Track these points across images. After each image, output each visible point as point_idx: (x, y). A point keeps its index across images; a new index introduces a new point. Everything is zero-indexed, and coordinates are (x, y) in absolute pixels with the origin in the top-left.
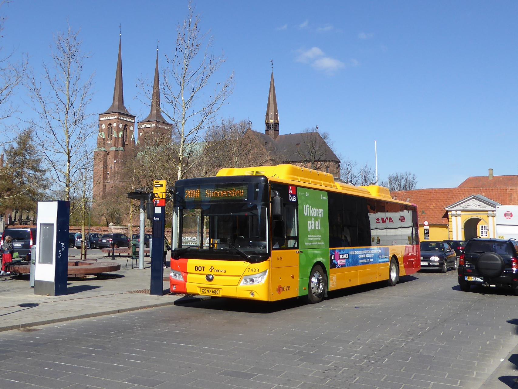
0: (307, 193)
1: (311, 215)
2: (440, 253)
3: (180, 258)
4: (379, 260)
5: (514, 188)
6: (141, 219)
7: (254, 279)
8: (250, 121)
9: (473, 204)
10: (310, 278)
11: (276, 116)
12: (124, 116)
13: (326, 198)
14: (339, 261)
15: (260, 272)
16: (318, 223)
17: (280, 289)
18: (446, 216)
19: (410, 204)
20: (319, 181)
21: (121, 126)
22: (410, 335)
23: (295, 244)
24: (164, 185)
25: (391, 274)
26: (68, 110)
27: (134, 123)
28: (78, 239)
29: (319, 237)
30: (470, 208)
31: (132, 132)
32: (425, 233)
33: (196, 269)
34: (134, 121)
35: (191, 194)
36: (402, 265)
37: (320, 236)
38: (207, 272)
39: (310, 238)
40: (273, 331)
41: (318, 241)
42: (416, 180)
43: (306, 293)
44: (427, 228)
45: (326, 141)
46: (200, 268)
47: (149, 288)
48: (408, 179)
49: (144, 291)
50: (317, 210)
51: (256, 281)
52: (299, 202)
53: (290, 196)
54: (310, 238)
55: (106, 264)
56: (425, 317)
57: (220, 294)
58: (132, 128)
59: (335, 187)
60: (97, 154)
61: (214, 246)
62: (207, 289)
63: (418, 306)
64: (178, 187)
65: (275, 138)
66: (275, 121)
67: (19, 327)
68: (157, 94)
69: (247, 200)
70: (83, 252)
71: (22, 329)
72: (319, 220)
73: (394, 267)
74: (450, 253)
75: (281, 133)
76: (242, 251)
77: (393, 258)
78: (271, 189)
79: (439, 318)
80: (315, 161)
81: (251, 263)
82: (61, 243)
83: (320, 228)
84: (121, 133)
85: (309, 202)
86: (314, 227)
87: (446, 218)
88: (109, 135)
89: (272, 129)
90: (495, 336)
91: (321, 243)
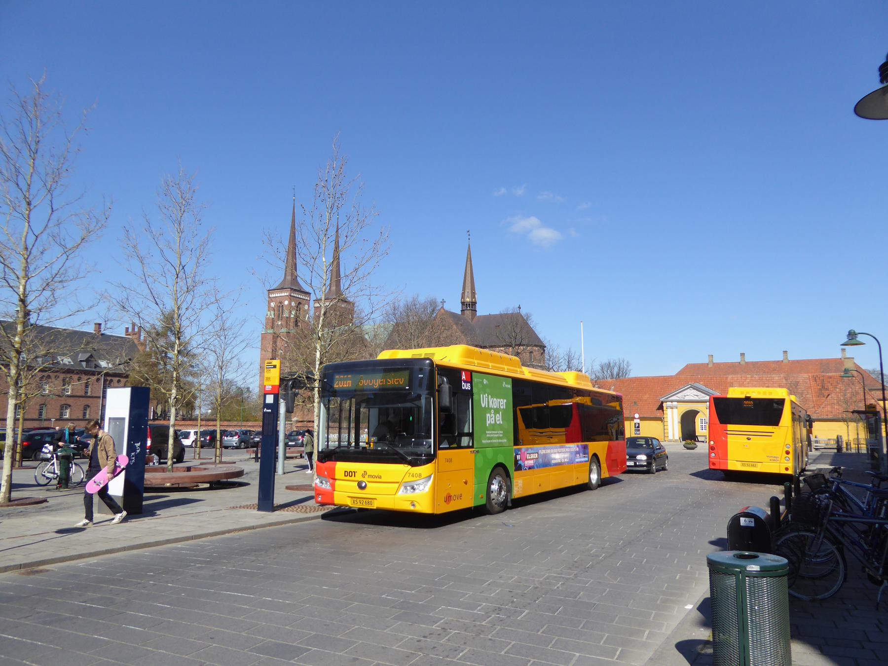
0: (485, 380)
1: (490, 407)
2: (648, 451)
3: (327, 461)
4: (577, 460)
5: (734, 376)
6: (280, 412)
7: (415, 486)
8: (443, 300)
9: (690, 394)
10: (490, 483)
11: (473, 294)
12: (297, 293)
13: (509, 386)
14: (526, 462)
15: (422, 478)
16: (499, 417)
17: (448, 499)
18: (661, 407)
19: (614, 393)
20: (502, 366)
21: (293, 304)
22: (576, 567)
23: (469, 443)
24: (278, 367)
25: (591, 476)
26: (179, 273)
27: (309, 301)
28: (225, 437)
29: (501, 434)
30: (687, 398)
31: (307, 312)
32: (635, 427)
33: (346, 475)
34: (309, 299)
35: (342, 383)
36: (604, 465)
37: (502, 432)
38: (359, 477)
39: (489, 434)
40: (386, 566)
41: (499, 438)
42: (630, 368)
43: (483, 502)
44: (638, 421)
45: (529, 322)
46: (351, 473)
47: (256, 501)
48: (622, 366)
49: (247, 507)
50: (499, 400)
51: (418, 489)
52: (475, 390)
53: (463, 383)
54: (489, 434)
55: (225, 469)
56: (605, 538)
57: (375, 505)
58: (306, 307)
59: (522, 373)
60: (264, 337)
61: (370, 445)
62: (358, 500)
63: (602, 521)
64: (327, 372)
65: (472, 319)
66: (472, 300)
67: (20, 566)
68: (293, 252)
69: (408, 388)
70: (218, 454)
71: (23, 570)
72: (501, 412)
73: (594, 468)
74: (660, 451)
75: (478, 314)
76: (401, 452)
77: (594, 457)
78: (438, 374)
79: (622, 539)
80: (516, 345)
81: (412, 466)
82: (134, 443)
83: (501, 423)
84: (293, 313)
85: (488, 390)
86: (494, 420)
87: (661, 411)
88: (279, 316)
89: (468, 308)
90: (689, 566)
91: (503, 441)
